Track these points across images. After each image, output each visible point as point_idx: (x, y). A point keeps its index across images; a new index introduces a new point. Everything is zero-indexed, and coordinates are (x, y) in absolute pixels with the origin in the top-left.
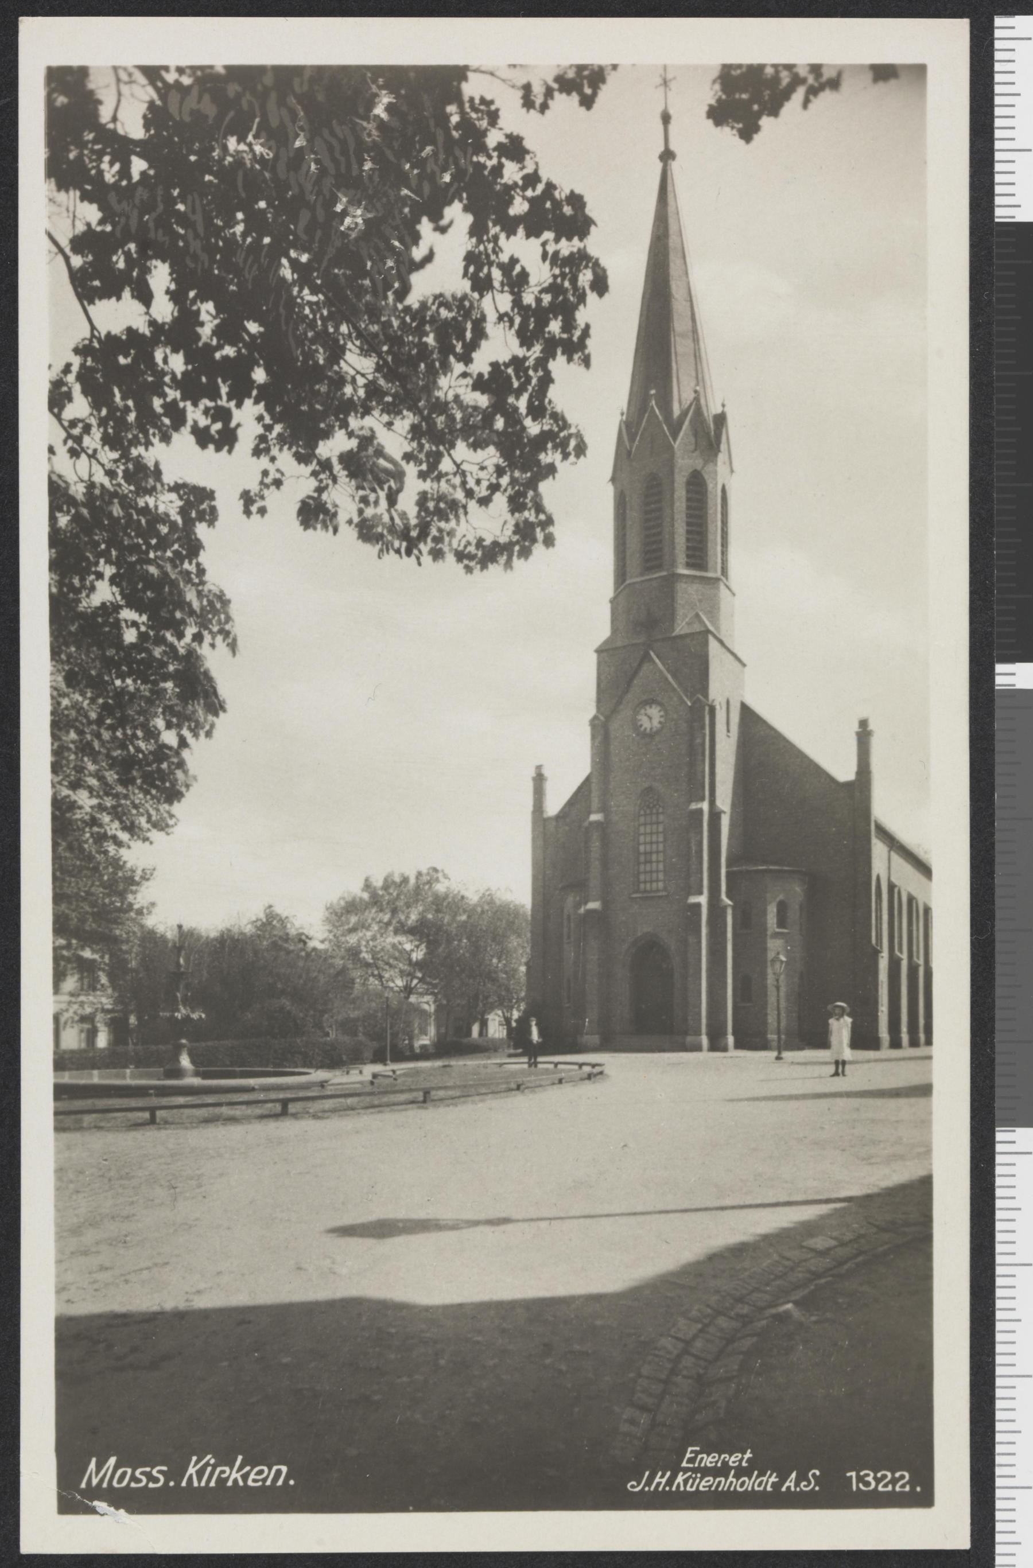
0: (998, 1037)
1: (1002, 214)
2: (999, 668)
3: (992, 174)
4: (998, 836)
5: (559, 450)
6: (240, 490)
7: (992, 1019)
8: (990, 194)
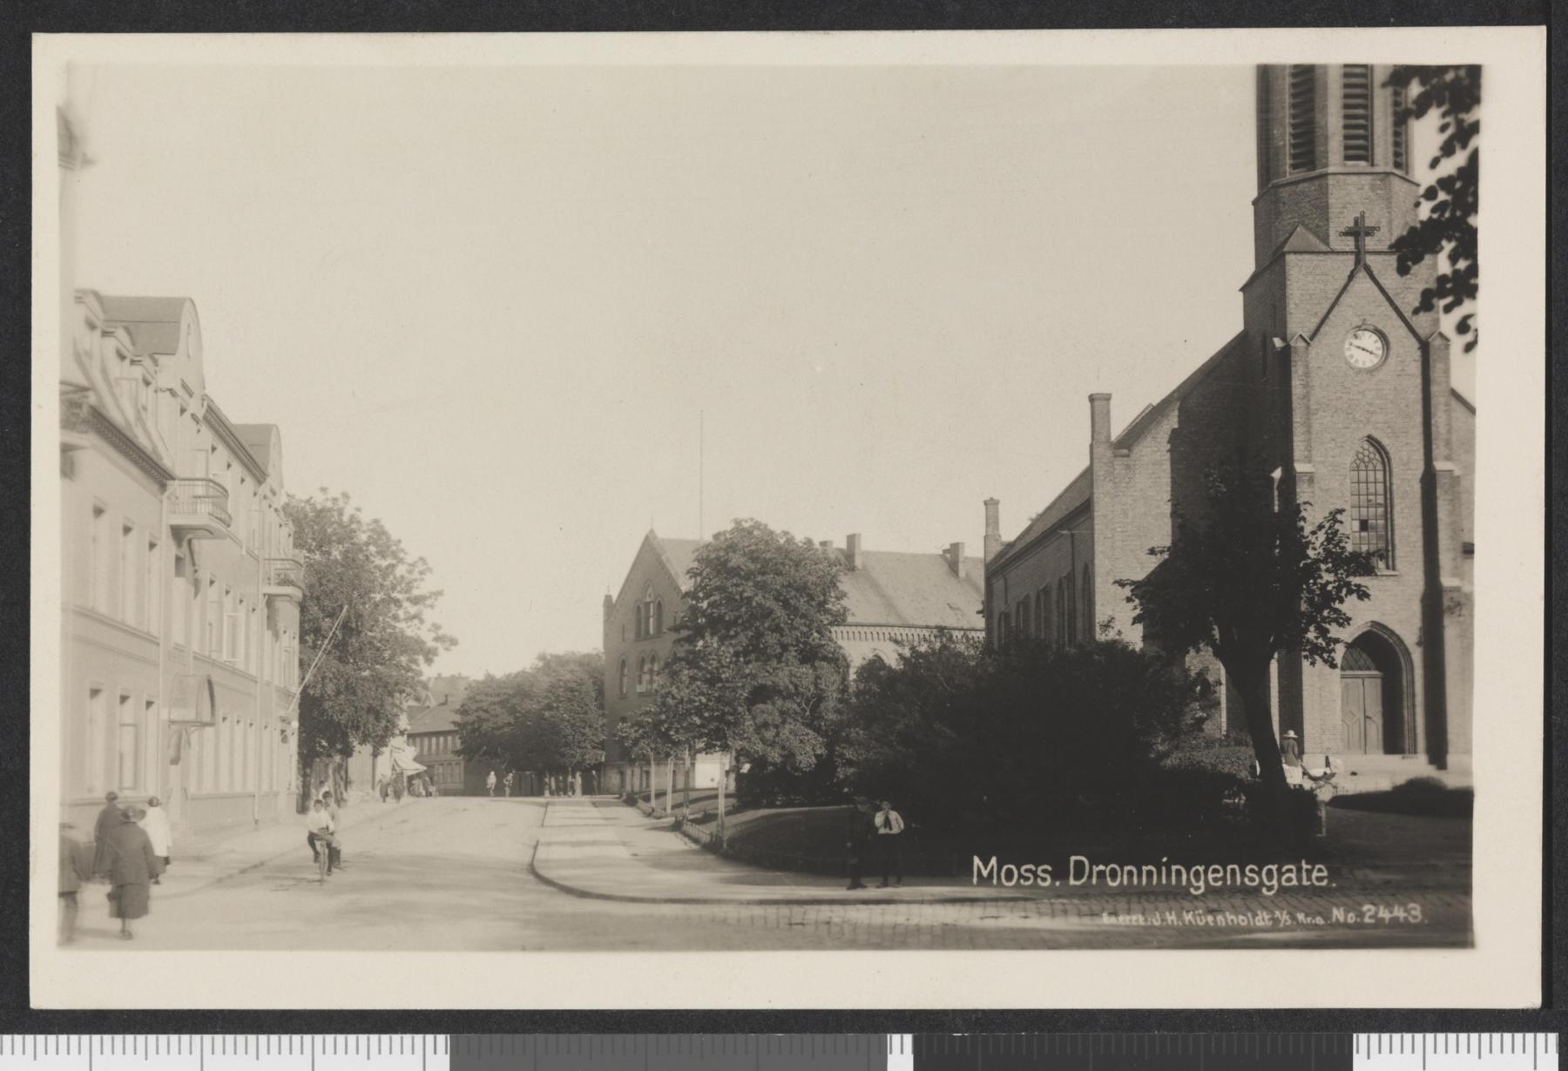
0: (541, 1037)
1: (1361, 1040)
2: (908, 1038)
3: (1401, 1030)
4: (740, 1037)
5: (1193, 674)
6: (851, 532)
7: (558, 1031)
8: (1381, 1029)
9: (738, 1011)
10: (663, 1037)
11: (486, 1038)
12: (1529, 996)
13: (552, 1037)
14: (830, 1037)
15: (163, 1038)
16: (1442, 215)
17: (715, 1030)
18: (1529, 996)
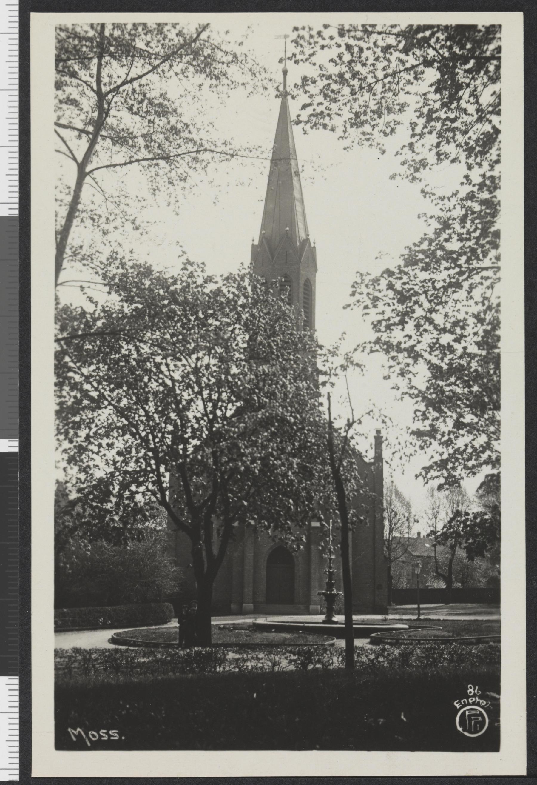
1: (15, 680)
2: (17, 450)
7: (20, 271)
9: (30, 230)
10: (17, 325)
11: (17, 234)
12: (37, 772)
13: (17, 268)
14: (17, 410)
15: (17, 155)
16: (172, 338)
17: (21, 351)
18: (37, 772)
